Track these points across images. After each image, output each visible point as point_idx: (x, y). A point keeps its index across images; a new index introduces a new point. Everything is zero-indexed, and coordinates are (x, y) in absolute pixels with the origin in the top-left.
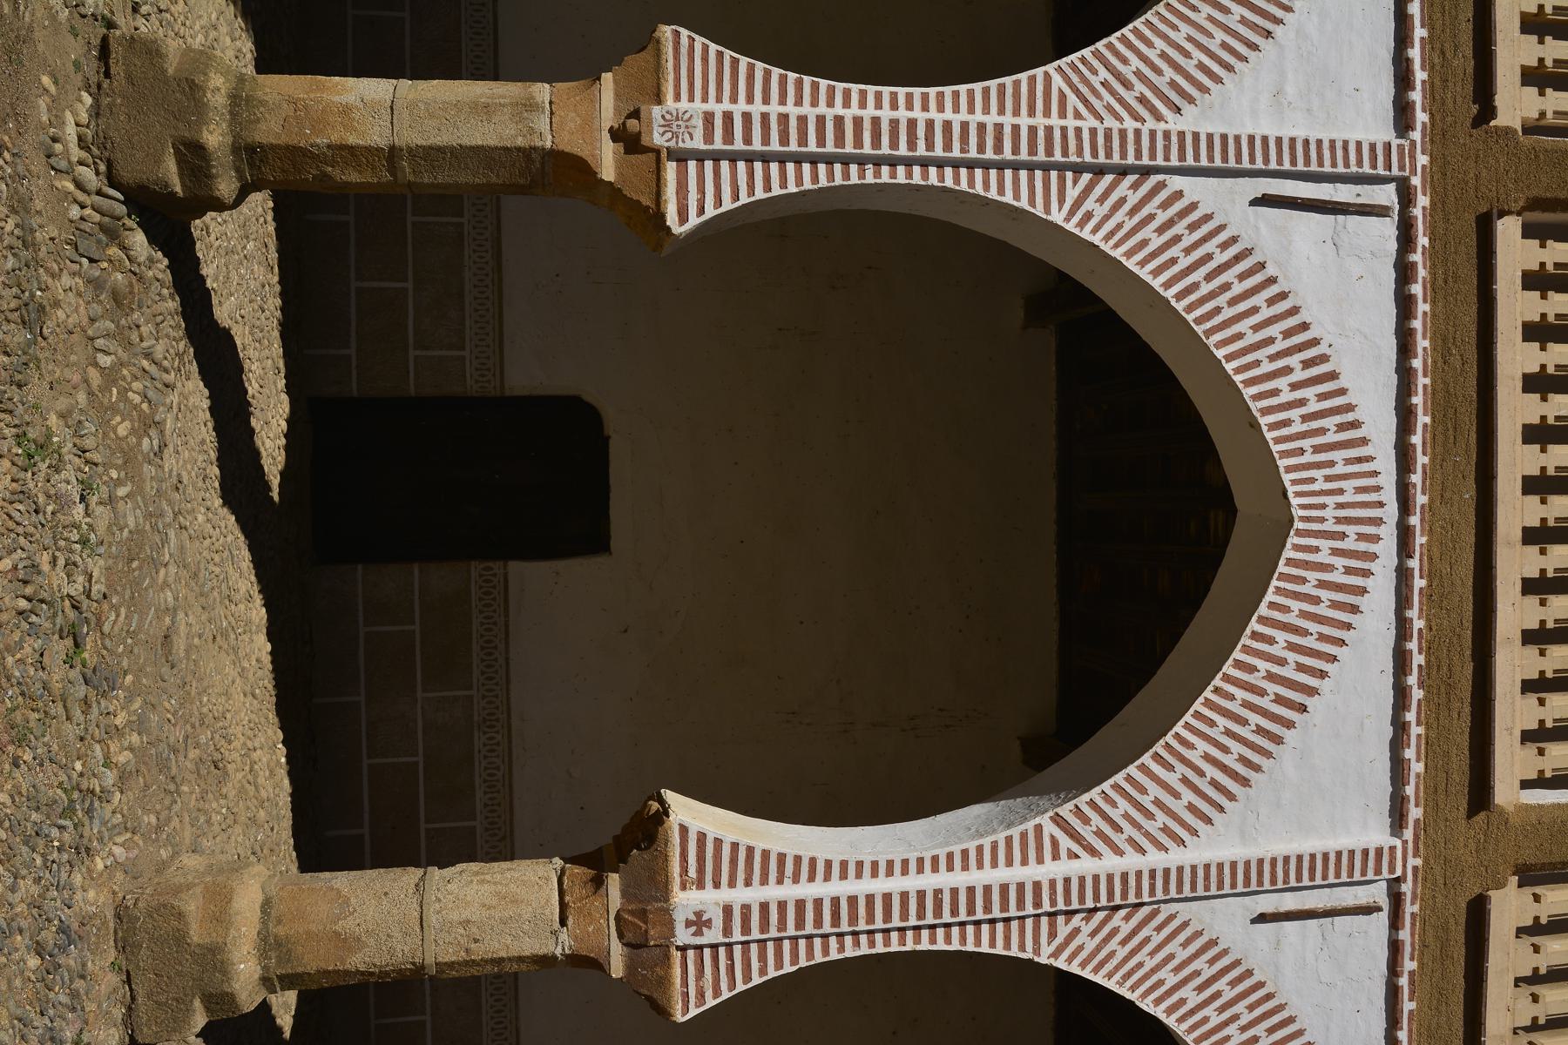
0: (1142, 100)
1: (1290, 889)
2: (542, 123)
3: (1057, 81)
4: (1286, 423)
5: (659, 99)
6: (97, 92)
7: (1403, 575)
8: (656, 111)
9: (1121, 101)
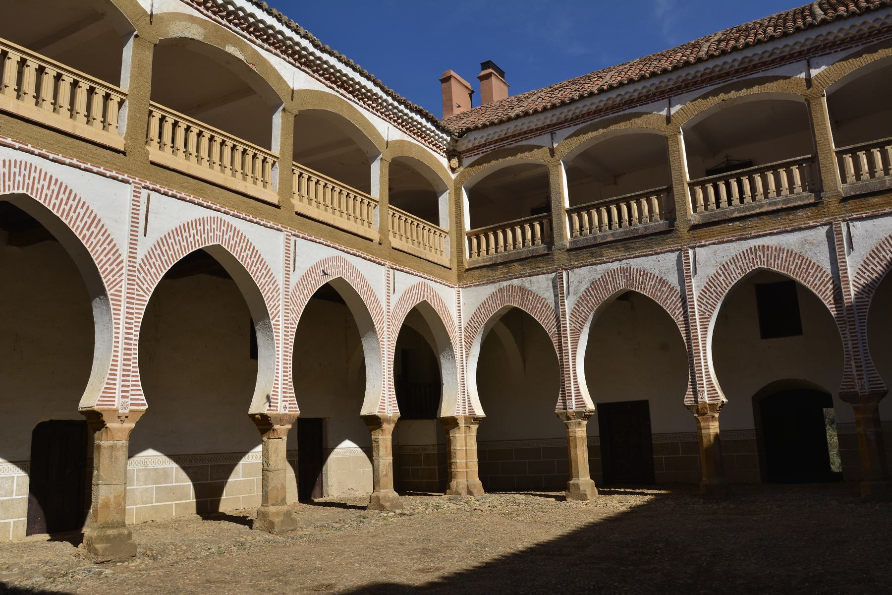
0: (117, 265)
1: (140, 222)
2: (120, 443)
3: (112, 291)
4: (9, 186)
5: (116, 410)
6: (116, 562)
7: (225, 213)
8: (120, 411)
9: (118, 272)
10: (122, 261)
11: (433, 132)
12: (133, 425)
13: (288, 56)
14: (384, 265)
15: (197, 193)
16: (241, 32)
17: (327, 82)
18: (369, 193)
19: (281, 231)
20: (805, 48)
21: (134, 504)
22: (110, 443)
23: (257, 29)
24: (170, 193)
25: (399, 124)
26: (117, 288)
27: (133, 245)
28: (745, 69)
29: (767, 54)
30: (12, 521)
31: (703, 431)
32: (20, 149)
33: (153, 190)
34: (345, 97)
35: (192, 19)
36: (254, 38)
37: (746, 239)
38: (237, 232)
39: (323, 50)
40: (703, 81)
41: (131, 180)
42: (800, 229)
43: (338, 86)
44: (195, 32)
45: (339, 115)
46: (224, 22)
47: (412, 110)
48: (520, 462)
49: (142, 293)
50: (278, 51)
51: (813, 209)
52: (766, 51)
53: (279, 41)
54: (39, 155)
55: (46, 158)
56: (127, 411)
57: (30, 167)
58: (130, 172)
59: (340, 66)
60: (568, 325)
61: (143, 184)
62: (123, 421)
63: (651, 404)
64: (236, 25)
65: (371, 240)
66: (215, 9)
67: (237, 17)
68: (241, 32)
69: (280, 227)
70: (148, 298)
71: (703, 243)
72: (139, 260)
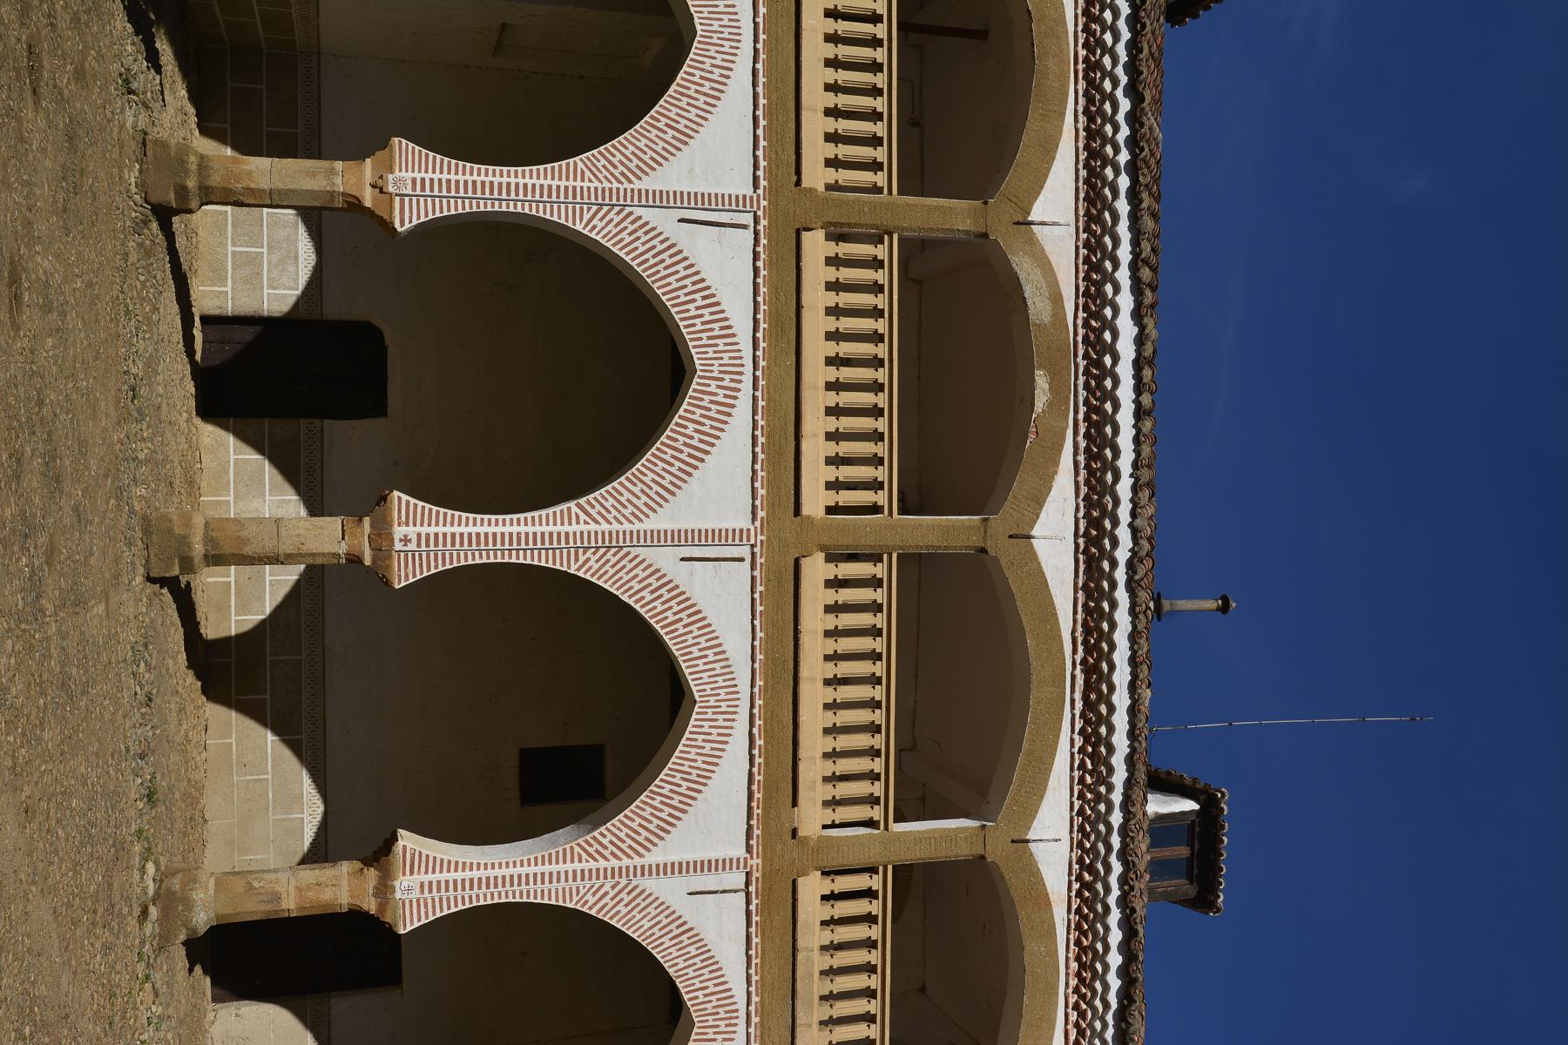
2: (338, 180)
3: (580, 165)
7: (755, 378)
8: (390, 177)
10: (630, 182)
11: (1106, 1005)
12: (368, 203)
13: (1087, 515)
15: (774, 317)
16: (1081, 400)
17: (1080, 629)
19: (754, 519)
21: (236, 497)
23: (1099, 426)
24: (760, 264)
25: (1079, 878)
26: (588, 173)
27: (662, 200)
30: (229, 289)
32: (756, 24)
33: (756, 233)
34: (1073, 691)
35: (1057, 299)
36: (1082, 430)
38: (727, 409)
39: (1131, 587)
41: (760, 191)
43: (1084, 662)
44: (1038, 307)
45: (1029, 674)
46: (1082, 363)
47: (1123, 901)
49: (586, 217)
50: (1084, 490)
53: (1101, 481)
54: (756, 50)
55: (755, 61)
56: (391, 189)
57: (736, 39)
59: (1121, 637)
61: (760, 213)
63: (381, 420)
64: (1087, 386)
65: (795, 804)
66: (1092, 337)
67: (1100, 380)
68: (1081, 400)
70: (579, 227)
72: (638, 211)
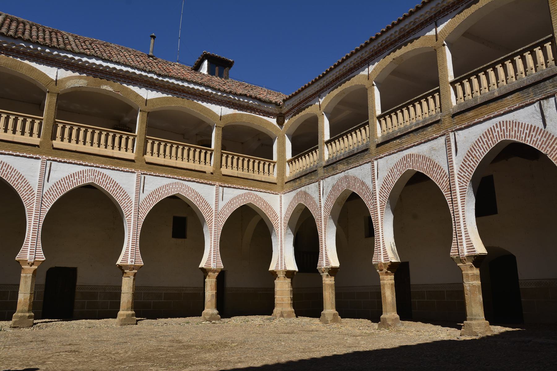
2: (29, 275)
14: (214, 185)
18: (210, 146)
20: (433, 14)
22: (24, 275)
24: (63, 160)
28: (404, 36)
29: (412, 23)
31: (381, 282)
33: (53, 160)
37: (402, 151)
40: (384, 49)
42: (429, 140)
48: (359, 303)
51: (436, 125)
52: (412, 22)
58: (40, 153)
60: (323, 214)
62: (31, 266)
65: (205, 172)
69: (133, 170)
71: (381, 155)
